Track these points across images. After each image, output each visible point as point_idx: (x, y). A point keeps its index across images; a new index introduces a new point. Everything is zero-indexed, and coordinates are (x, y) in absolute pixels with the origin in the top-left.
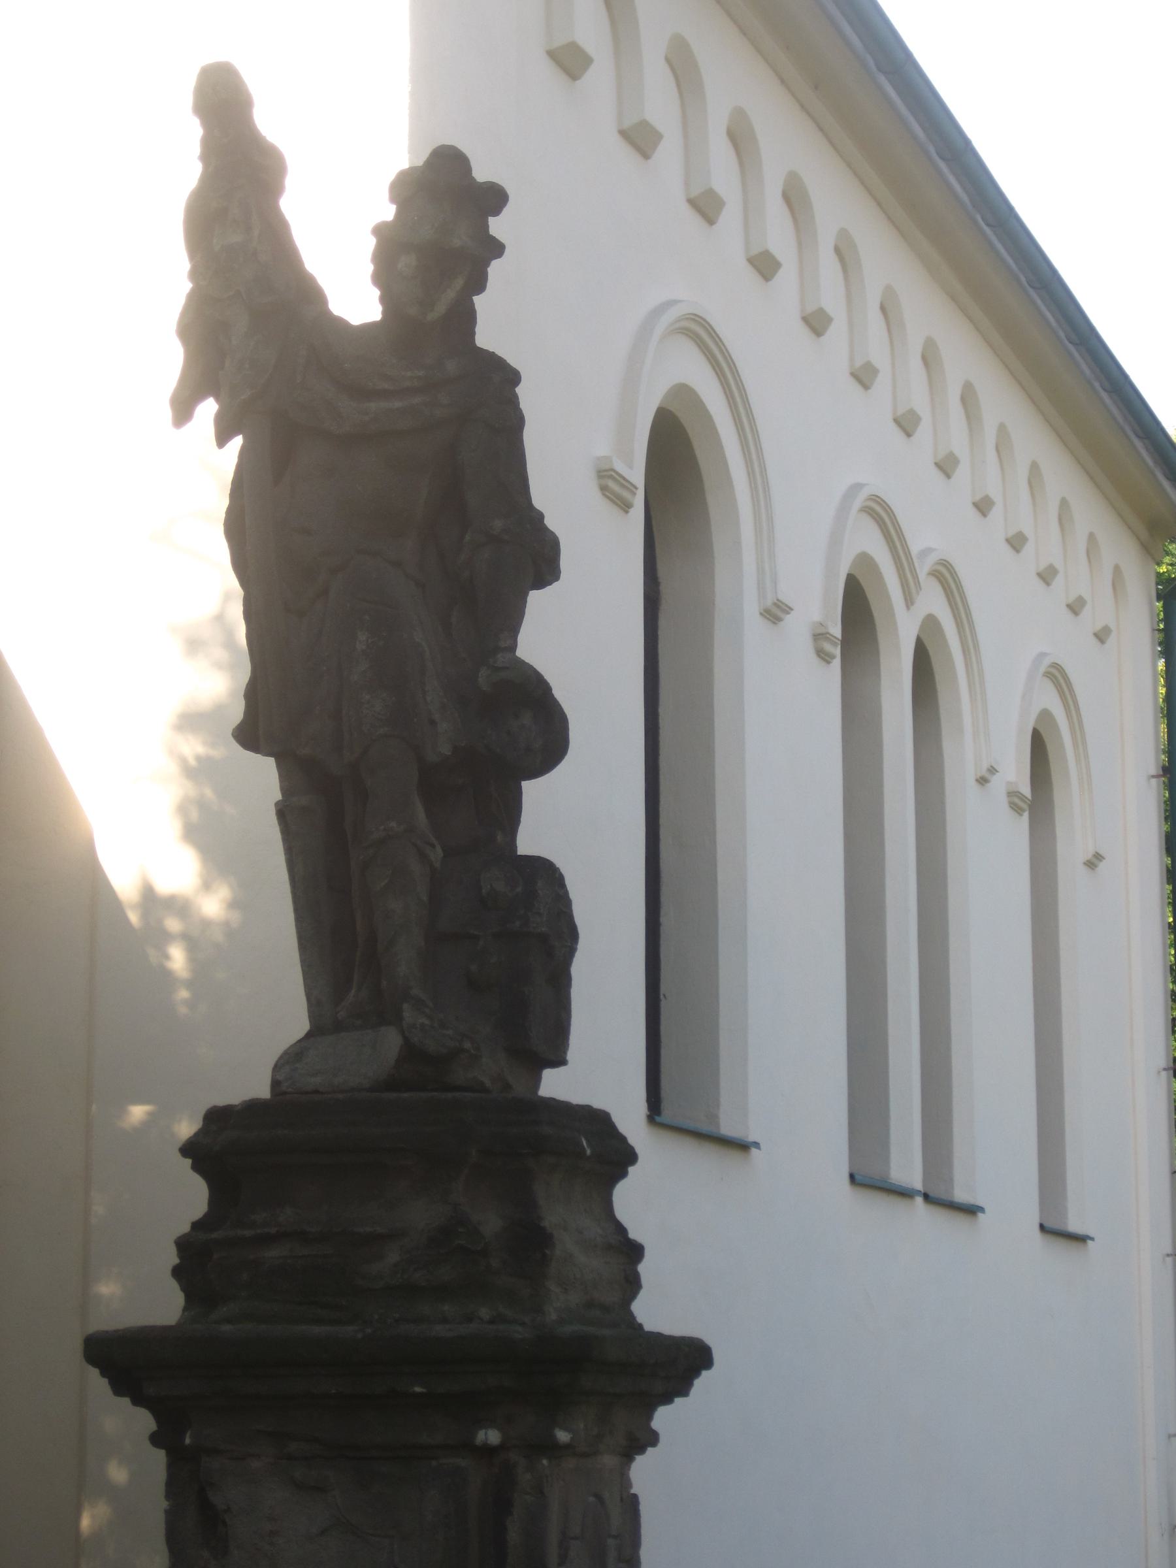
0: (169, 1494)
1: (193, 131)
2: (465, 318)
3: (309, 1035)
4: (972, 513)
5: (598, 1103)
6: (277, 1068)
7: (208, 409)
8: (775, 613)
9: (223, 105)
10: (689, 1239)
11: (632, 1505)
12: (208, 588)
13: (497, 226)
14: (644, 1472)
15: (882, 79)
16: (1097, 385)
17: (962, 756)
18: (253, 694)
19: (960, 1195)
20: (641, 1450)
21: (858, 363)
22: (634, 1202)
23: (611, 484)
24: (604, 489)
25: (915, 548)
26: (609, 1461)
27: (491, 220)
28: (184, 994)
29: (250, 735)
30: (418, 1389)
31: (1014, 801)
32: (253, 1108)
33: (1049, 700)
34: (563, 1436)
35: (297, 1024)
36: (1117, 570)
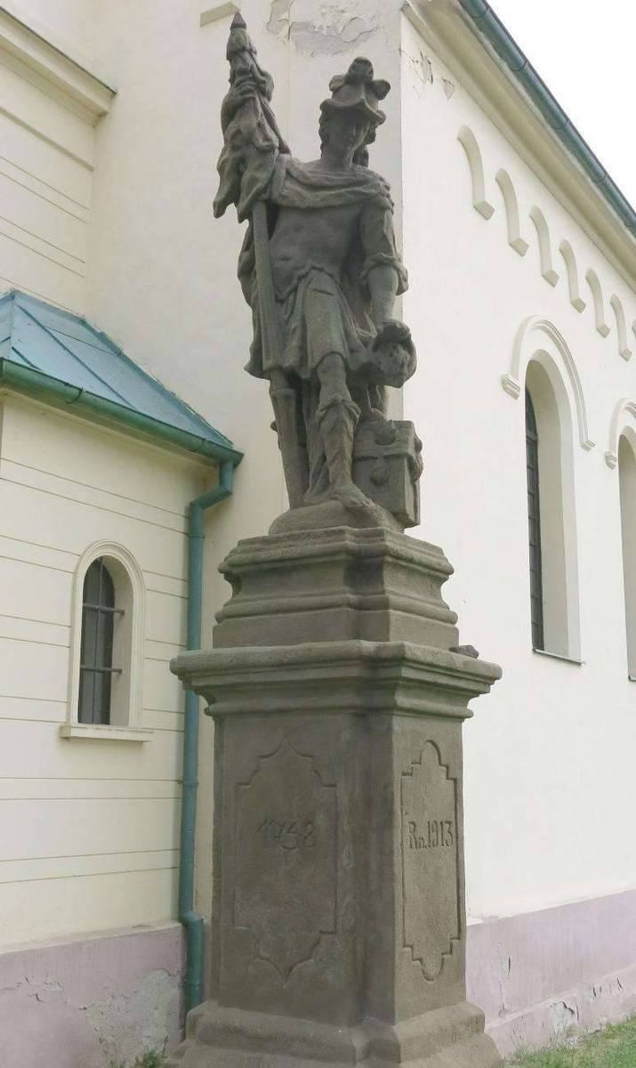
21: (623, 350)
23: (509, 387)
24: (505, 389)
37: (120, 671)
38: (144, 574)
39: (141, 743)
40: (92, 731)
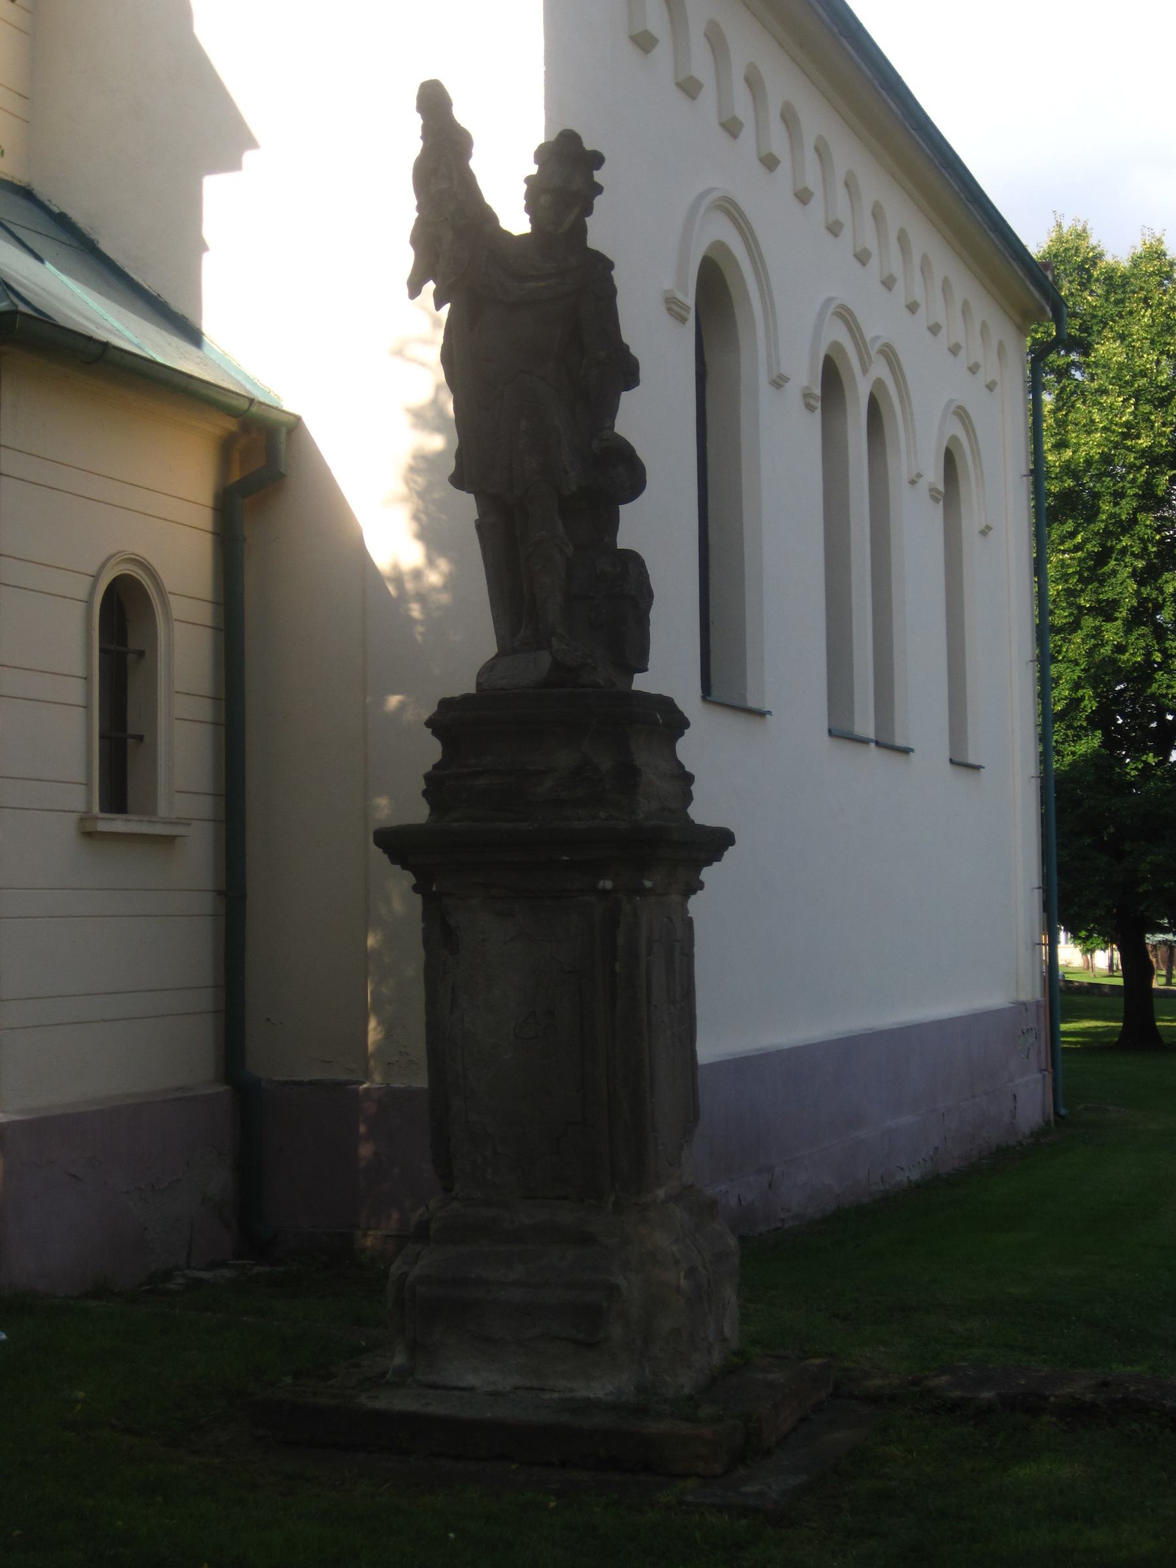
0: (424, 919)
1: (416, 122)
2: (580, 231)
3: (497, 656)
4: (905, 311)
5: (666, 693)
6: (479, 675)
7: (430, 287)
8: (779, 382)
9: (434, 103)
10: (718, 770)
11: (689, 924)
12: (423, 378)
13: (598, 176)
14: (696, 905)
15: (843, 40)
16: (986, 227)
17: (899, 467)
18: (460, 455)
19: (899, 742)
20: (694, 892)
22: (687, 750)
24: (669, 310)
25: (868, 337)
26: (675, 898)
27: (595, 172)
28: (420, 629)
29: (458, 480)
30: (565, 858)
31: (934, 494)
32: (466, 698)
33: (957, 430)
34: (648, 884)
35: (488, 648)
36: (1001, 344)
37: (140, 738)
38: (170, 597)
39: (171, 839)
40: (118, 824)
